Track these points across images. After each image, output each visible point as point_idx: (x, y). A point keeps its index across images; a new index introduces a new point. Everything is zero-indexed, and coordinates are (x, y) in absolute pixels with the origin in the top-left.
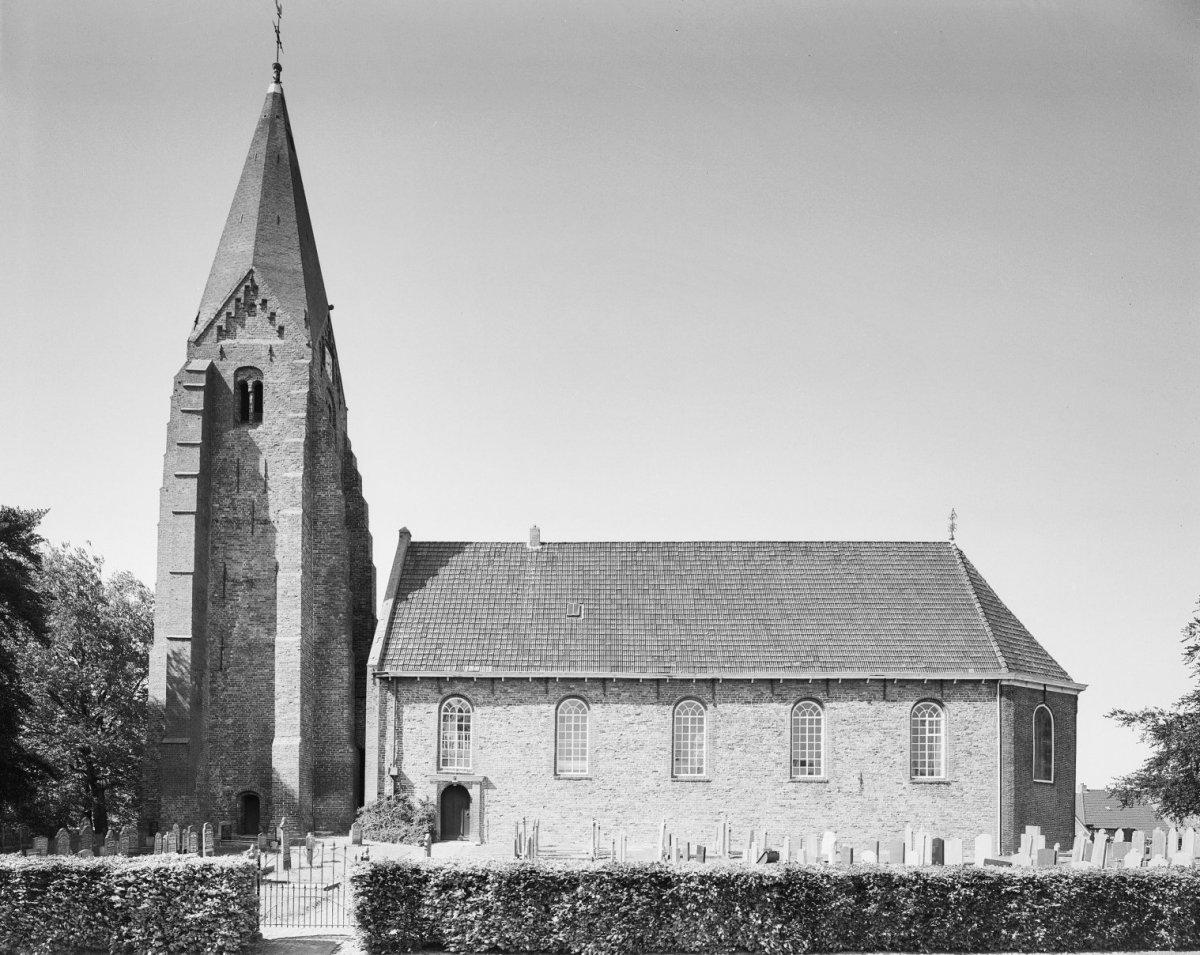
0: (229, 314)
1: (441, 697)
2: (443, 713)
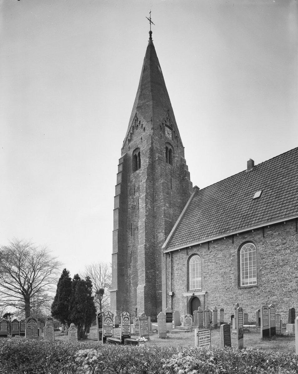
1: (188, 257)
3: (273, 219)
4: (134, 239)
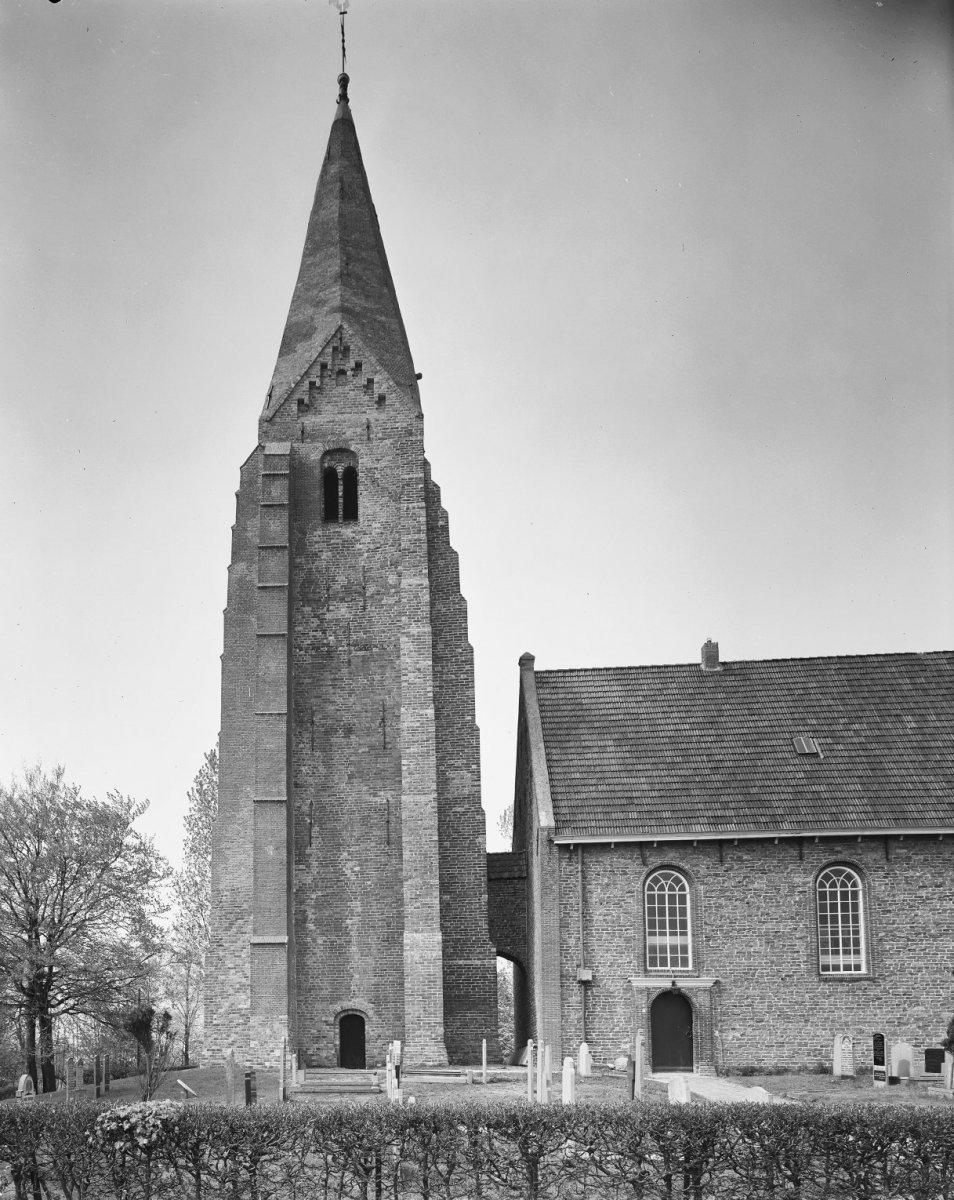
0: (312, 384)
1: (646, 870)
2: (647, 893)
3: (920, 823)
4: (328, 765)
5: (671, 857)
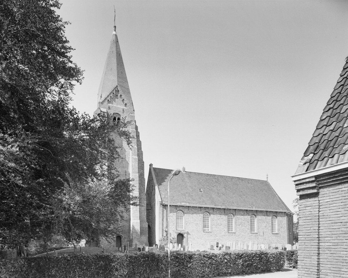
5: (181, 208)
